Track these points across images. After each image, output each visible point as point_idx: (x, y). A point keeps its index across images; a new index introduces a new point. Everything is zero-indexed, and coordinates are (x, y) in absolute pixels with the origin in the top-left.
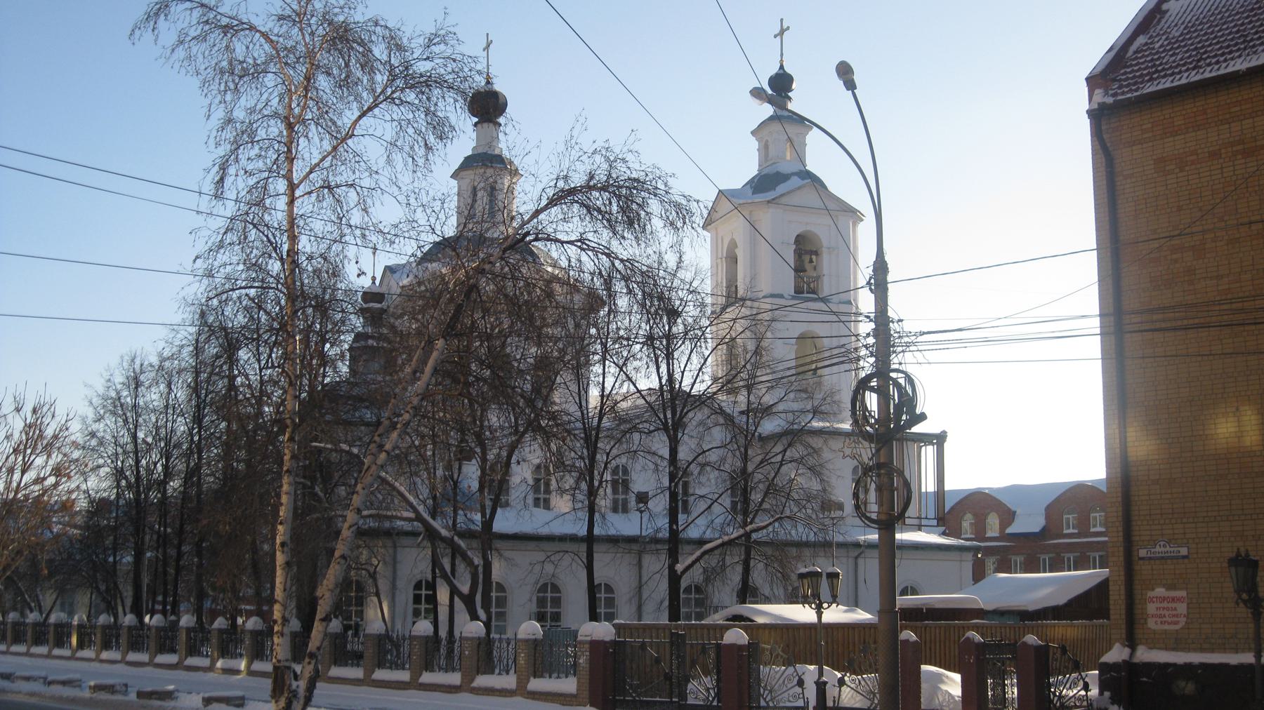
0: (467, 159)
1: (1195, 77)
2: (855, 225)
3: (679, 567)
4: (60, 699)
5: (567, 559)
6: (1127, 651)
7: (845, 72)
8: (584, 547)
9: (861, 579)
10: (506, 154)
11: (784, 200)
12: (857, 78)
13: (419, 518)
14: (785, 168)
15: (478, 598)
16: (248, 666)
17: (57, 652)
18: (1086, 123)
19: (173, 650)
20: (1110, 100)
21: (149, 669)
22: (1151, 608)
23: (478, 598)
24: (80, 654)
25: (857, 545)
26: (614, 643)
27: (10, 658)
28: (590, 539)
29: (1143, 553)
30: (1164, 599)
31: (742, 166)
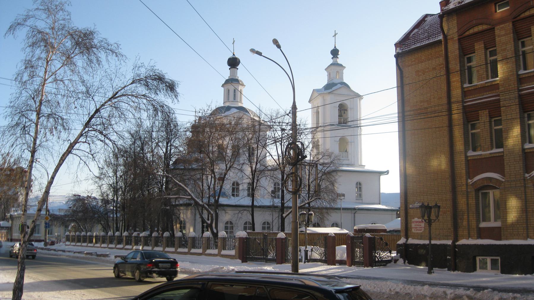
0: (227, 80)
1: (427, 42)
2: (360, 100)
3: (284, 215)
4: (78, 257)
5: (245, 212)
6: (405, 240)
7: (275, 42)
8: (250, 209)
9: (245, 208)
10: (239, 79)
11: (335, 92)
12: (280, 43)
13: (192, 199)
14: (336, 81)
15: (214, 225)
16: (142, 248)
17: (89, 245)
18: (394, 60)
19: (131, 244)
20: (400, 51)
21: (115, 250)
22: (413, 225)
23: (214, 225)
24: (96, 245)
25: (355, 209)
26: (246, 238)
27: (76, 247)
28: (253, 206)
29: (411, 206)
30: (417, 222)
31: (322, 81)
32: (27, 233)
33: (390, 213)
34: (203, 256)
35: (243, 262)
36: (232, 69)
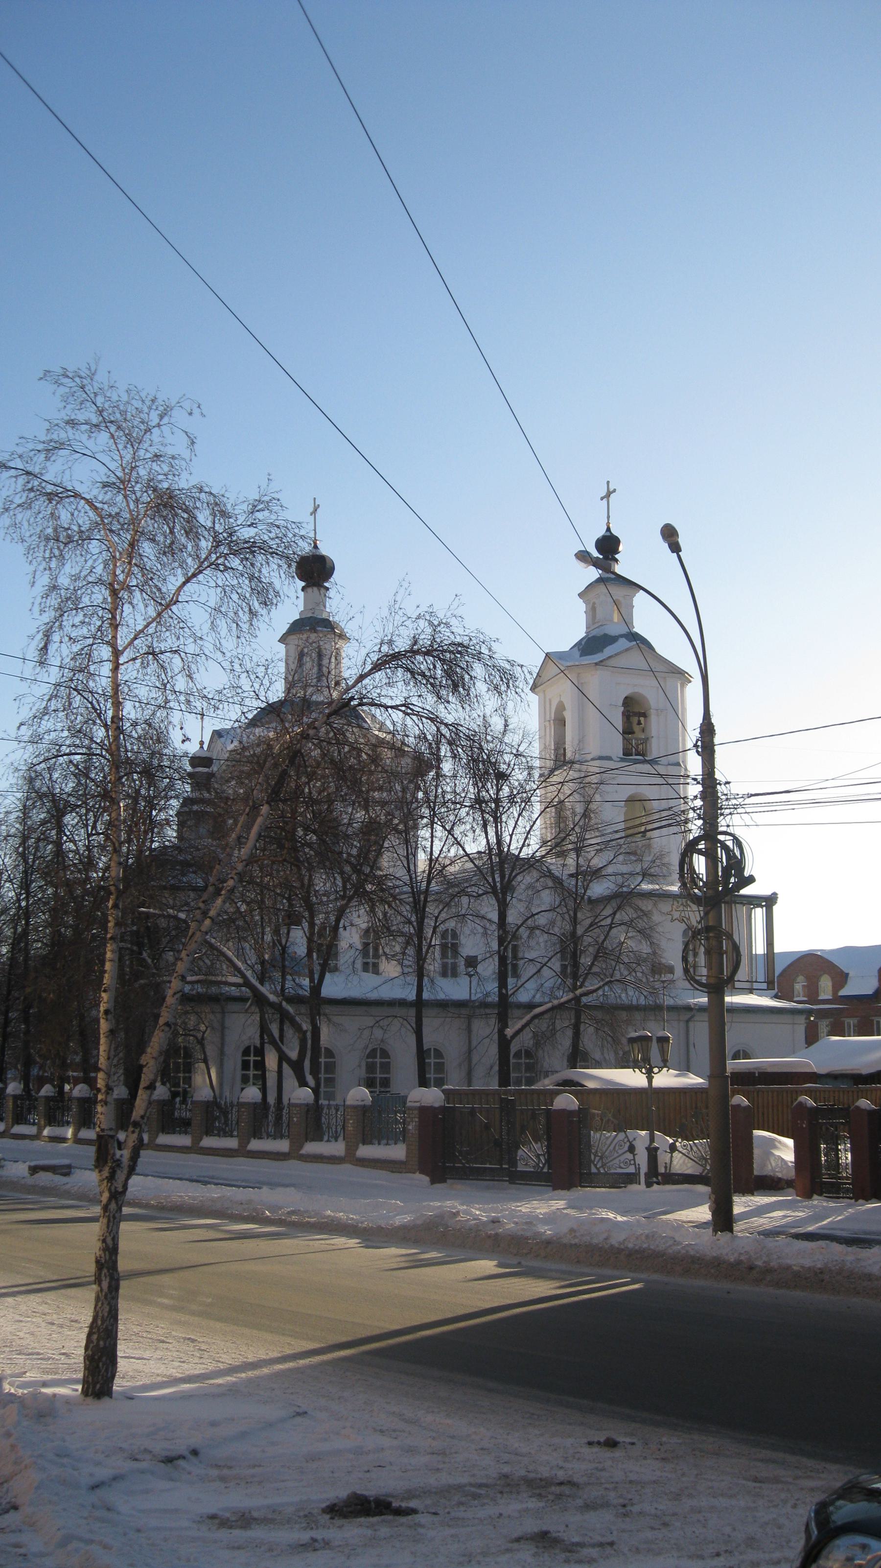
2: (683, 686)
3: (509, 1032)
5: (397, 1023)
7: (670, 534)
8: (412, 1012)
11: (612, 662)
12: (682, 541)
13: (247, 983)
14: (613, 631)
15: (307, 1064)
23: (307, 1064)
26: (443, 1109)
28: (419, 1004)
31: (569, 628)
32: (118, 1163)
33: (787, 1018)
34: (293, 1163)
35: (433, 1182)
36: (309, 590)
